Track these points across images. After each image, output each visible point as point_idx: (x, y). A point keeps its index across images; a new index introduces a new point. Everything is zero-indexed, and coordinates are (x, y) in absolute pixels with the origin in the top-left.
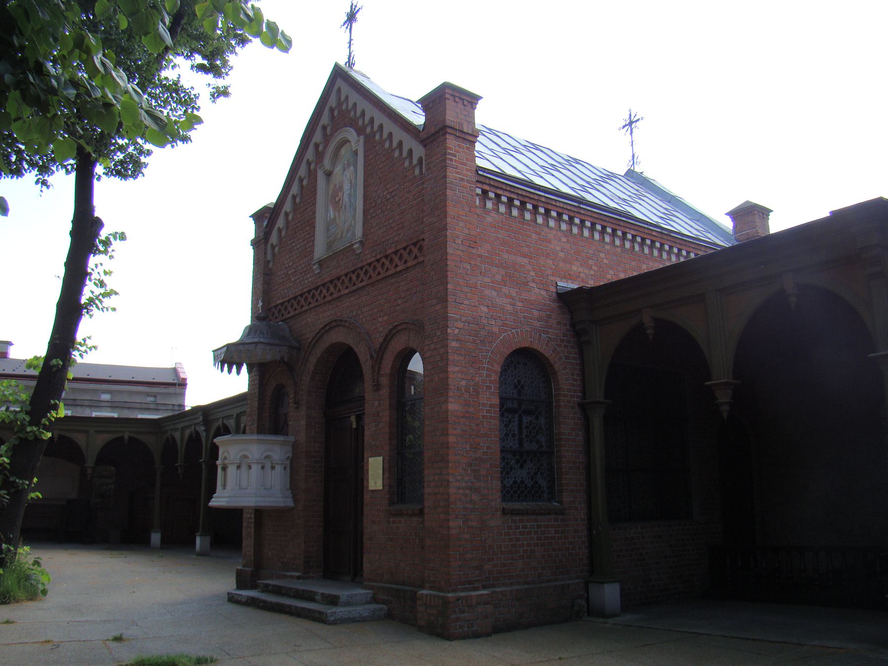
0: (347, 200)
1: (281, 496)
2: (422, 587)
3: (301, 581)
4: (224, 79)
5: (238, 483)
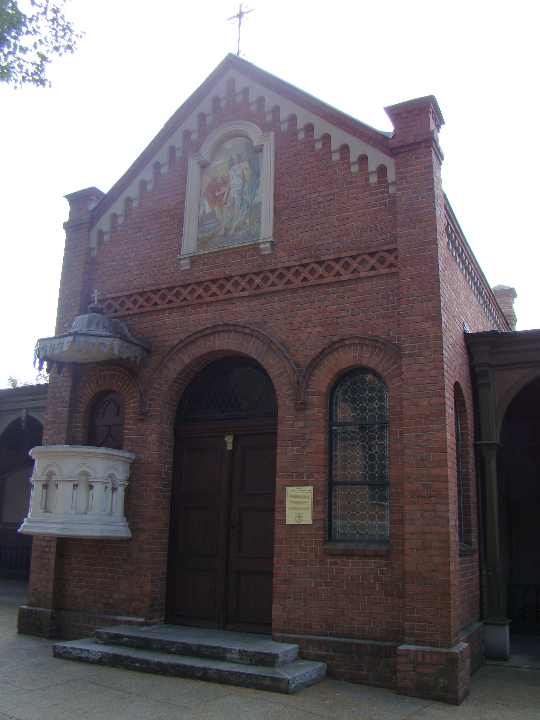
0: (236, 196)
1: (123, 524)
2: (403, 642)
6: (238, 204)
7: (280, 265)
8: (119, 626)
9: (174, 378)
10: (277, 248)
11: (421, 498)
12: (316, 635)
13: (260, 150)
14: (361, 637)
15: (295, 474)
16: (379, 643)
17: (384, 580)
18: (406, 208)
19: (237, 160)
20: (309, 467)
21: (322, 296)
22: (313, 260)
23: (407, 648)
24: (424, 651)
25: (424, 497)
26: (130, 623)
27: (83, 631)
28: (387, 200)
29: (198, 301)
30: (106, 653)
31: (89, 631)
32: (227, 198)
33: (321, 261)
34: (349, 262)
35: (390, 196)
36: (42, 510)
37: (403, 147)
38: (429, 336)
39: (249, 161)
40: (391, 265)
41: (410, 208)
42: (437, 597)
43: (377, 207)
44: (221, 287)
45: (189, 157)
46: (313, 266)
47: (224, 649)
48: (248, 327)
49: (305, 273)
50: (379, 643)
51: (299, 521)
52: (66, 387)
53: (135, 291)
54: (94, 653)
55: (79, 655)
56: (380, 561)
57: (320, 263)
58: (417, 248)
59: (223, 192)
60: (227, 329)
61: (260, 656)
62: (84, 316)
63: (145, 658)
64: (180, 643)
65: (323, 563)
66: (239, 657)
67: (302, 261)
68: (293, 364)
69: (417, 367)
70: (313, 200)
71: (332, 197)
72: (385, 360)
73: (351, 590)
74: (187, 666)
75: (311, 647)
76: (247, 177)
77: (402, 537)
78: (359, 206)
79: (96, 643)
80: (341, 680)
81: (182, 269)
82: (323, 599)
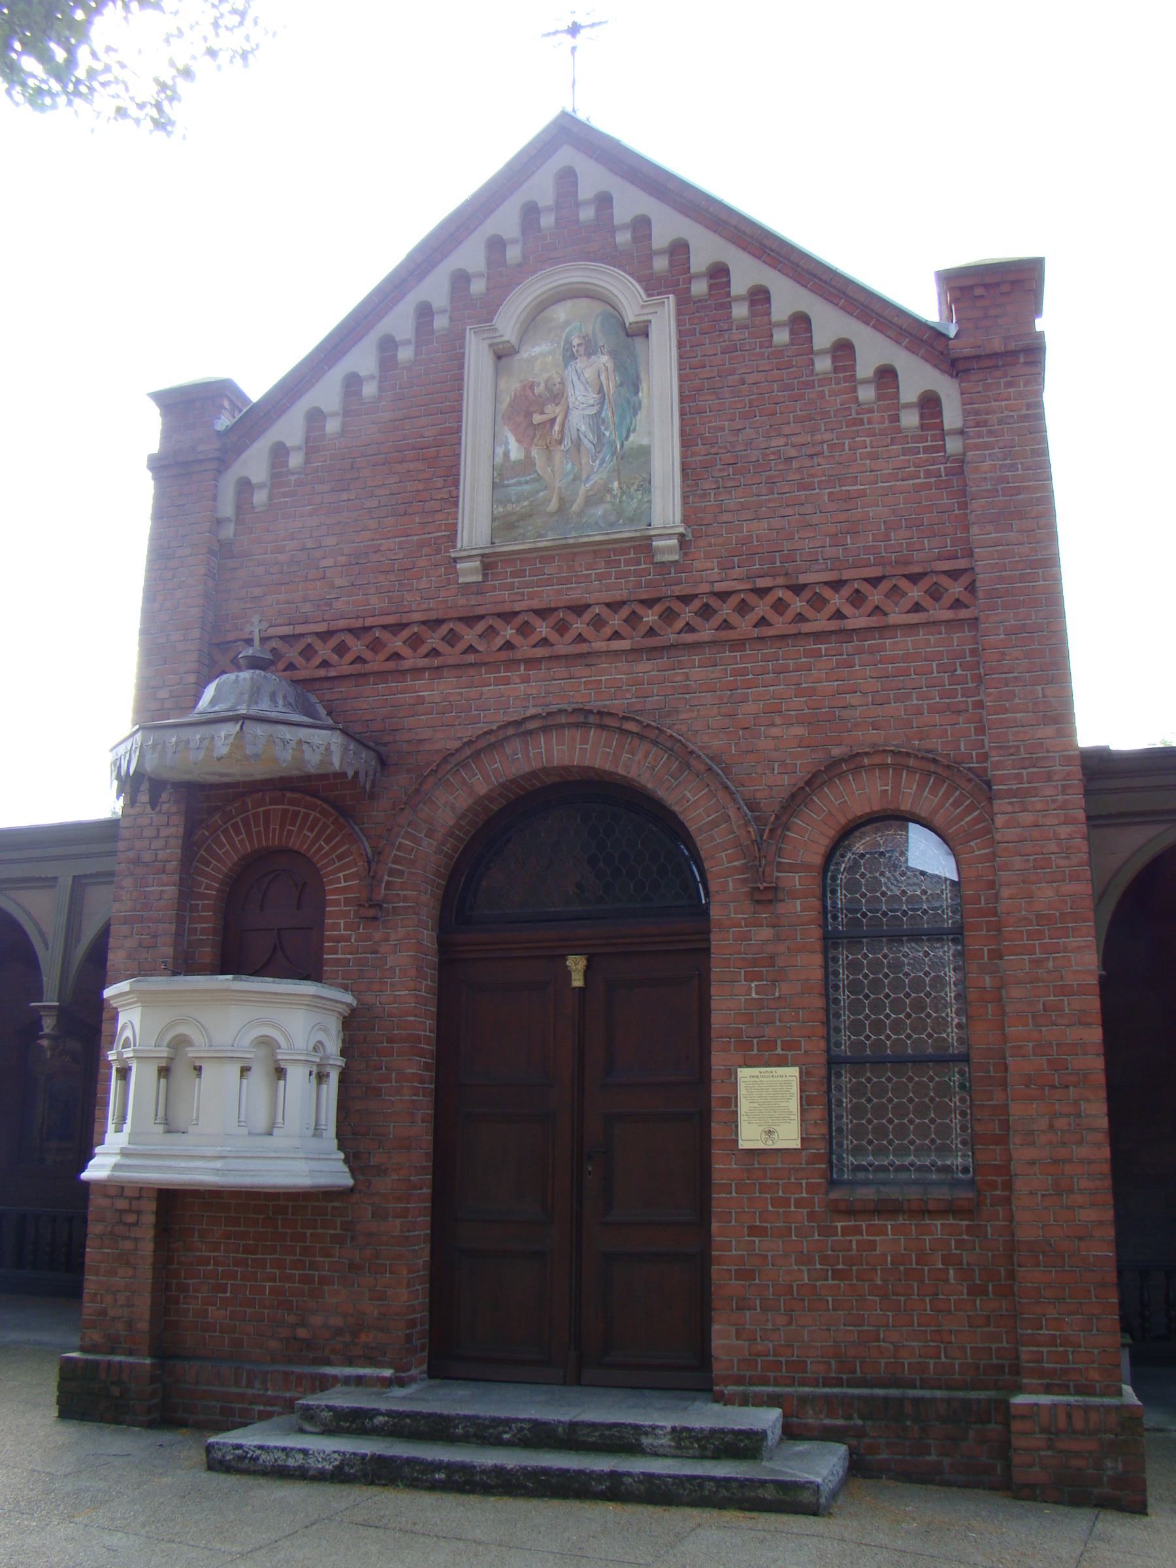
0: (583, 428)
2: (1019, 1389)
3: (352, 1389)
4: (172, 64)
5: (161, 1113)
6: (590, 446)
7: (704, 588)
8: (331, 1391)
9: (451, 824)
10: (693, 550)
11: (1047, 1088)
12: (817, 1386)
13: (642, 331)
14: (918, 1383)
15: (755, 1041)
16: (960, 1394)
17: (965, 1262)
18: (989, 487)
19: (582, 349)
20: (788, 1025)
21: (804, 660)
22: (780, 581)
23: (1033, 1402)
24: (1069, 1405)
25: (1053, 1087)
26: (359, 1381)
27: (233, 1405)
28: (942, 466)
29: (504, 655)
30: (355, 1454)
31: (251, 1403)
32: (562, 431)
33: (799, 585)
34: (862, 590)
35: (947, 459)
36: (161, 1128)
37: (978, 357)
38: (1051, 754)
39: (613, 354)
40: (957, 604)
41: (999, 487)
42: (1089, 1291)
43: (920, 478)
44: (562, 628)
45: (468, 331)
46: (780, 593)
47: (636, 1427)
48: (634, 719)
49: (762, 608)
50: (960, 1394)
51: (770, 1142)
52: (168, 837)
53: (342, 624)
54: (322, 1455)
55: (280, 1462)
56: (880, 1222)
57: (797, 589)
58: (1017, 573)
59: (552, 416)
60: (582, 719)
61: (722, 1439)
62: (237, 676)
63: (458, 1459)
64: (524, 1420)
65: (827, 1231)
66: (673, 1444)
67: (754, 582)
68: (742, 803)
69: (1027, 818)
70: (772, 453)
71: (818, 449)
72: (951, 800)
73: (892, 1285)
74: (568, 1470)
75: (811, 1412)
76: (609, 389)
77: (1004, 1169)
78: (879, 473)
79: (302, 1431)
80: (881, 1478)
81: (461, 580)
82: (831, 1307)
